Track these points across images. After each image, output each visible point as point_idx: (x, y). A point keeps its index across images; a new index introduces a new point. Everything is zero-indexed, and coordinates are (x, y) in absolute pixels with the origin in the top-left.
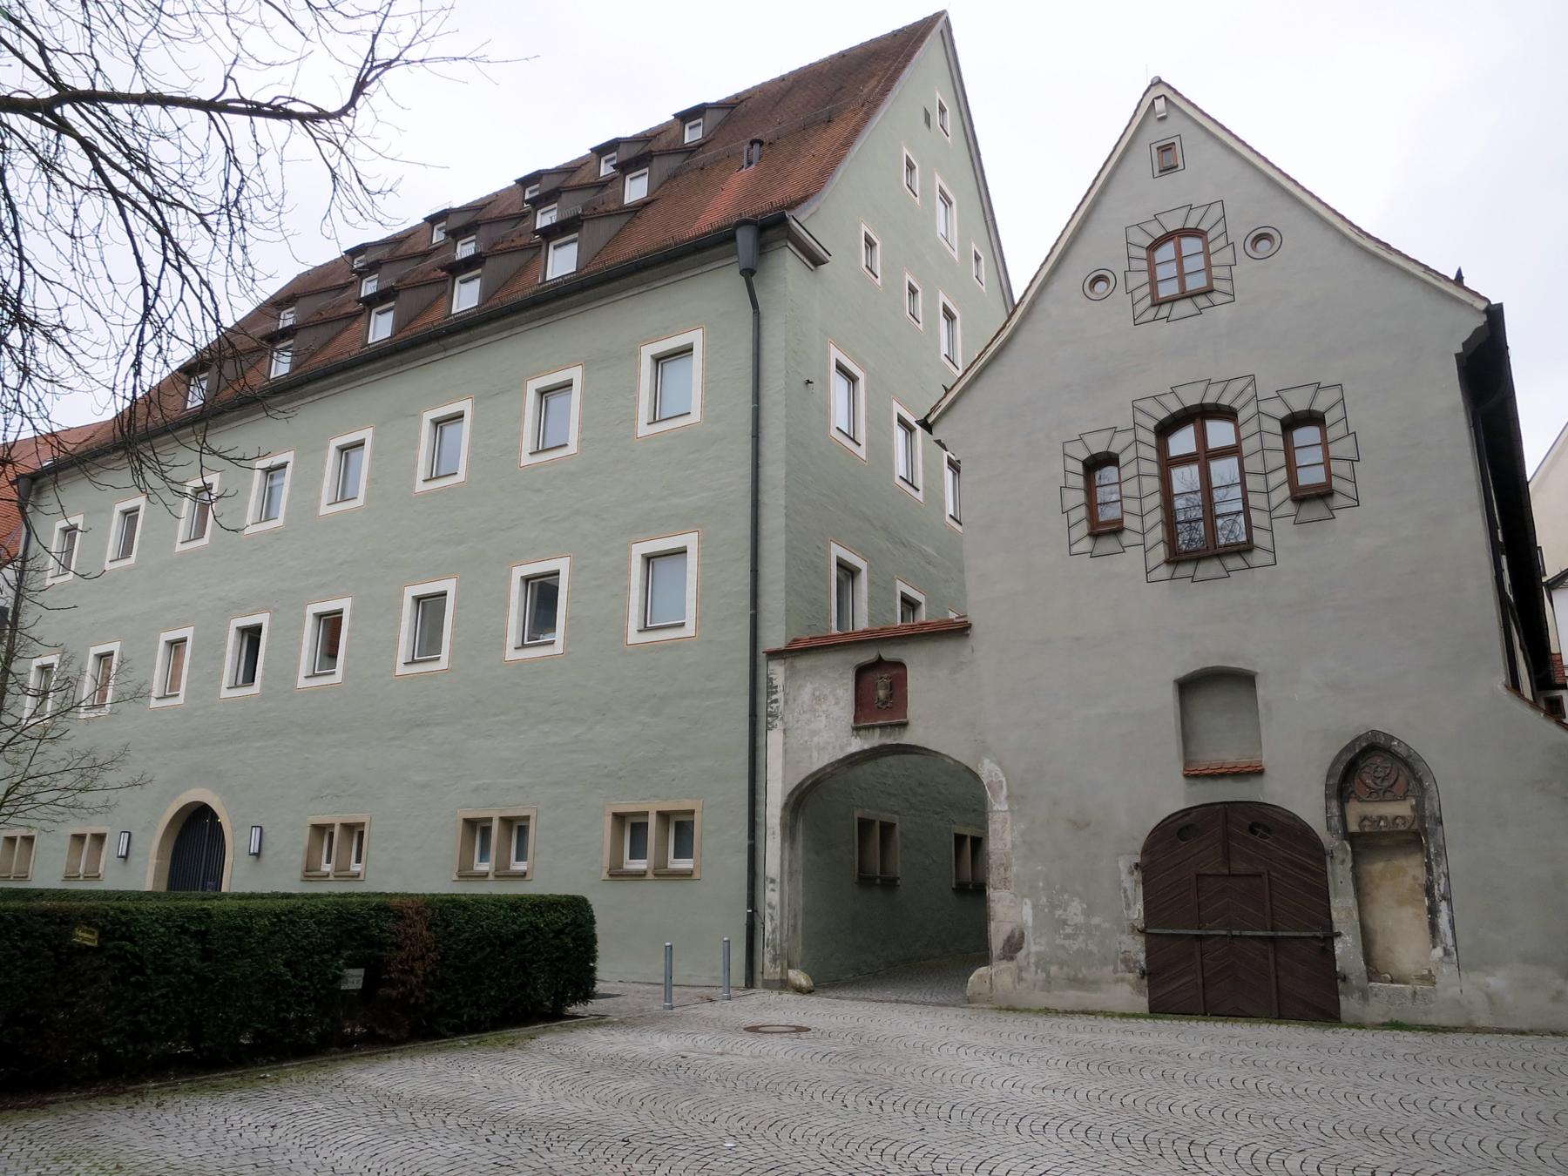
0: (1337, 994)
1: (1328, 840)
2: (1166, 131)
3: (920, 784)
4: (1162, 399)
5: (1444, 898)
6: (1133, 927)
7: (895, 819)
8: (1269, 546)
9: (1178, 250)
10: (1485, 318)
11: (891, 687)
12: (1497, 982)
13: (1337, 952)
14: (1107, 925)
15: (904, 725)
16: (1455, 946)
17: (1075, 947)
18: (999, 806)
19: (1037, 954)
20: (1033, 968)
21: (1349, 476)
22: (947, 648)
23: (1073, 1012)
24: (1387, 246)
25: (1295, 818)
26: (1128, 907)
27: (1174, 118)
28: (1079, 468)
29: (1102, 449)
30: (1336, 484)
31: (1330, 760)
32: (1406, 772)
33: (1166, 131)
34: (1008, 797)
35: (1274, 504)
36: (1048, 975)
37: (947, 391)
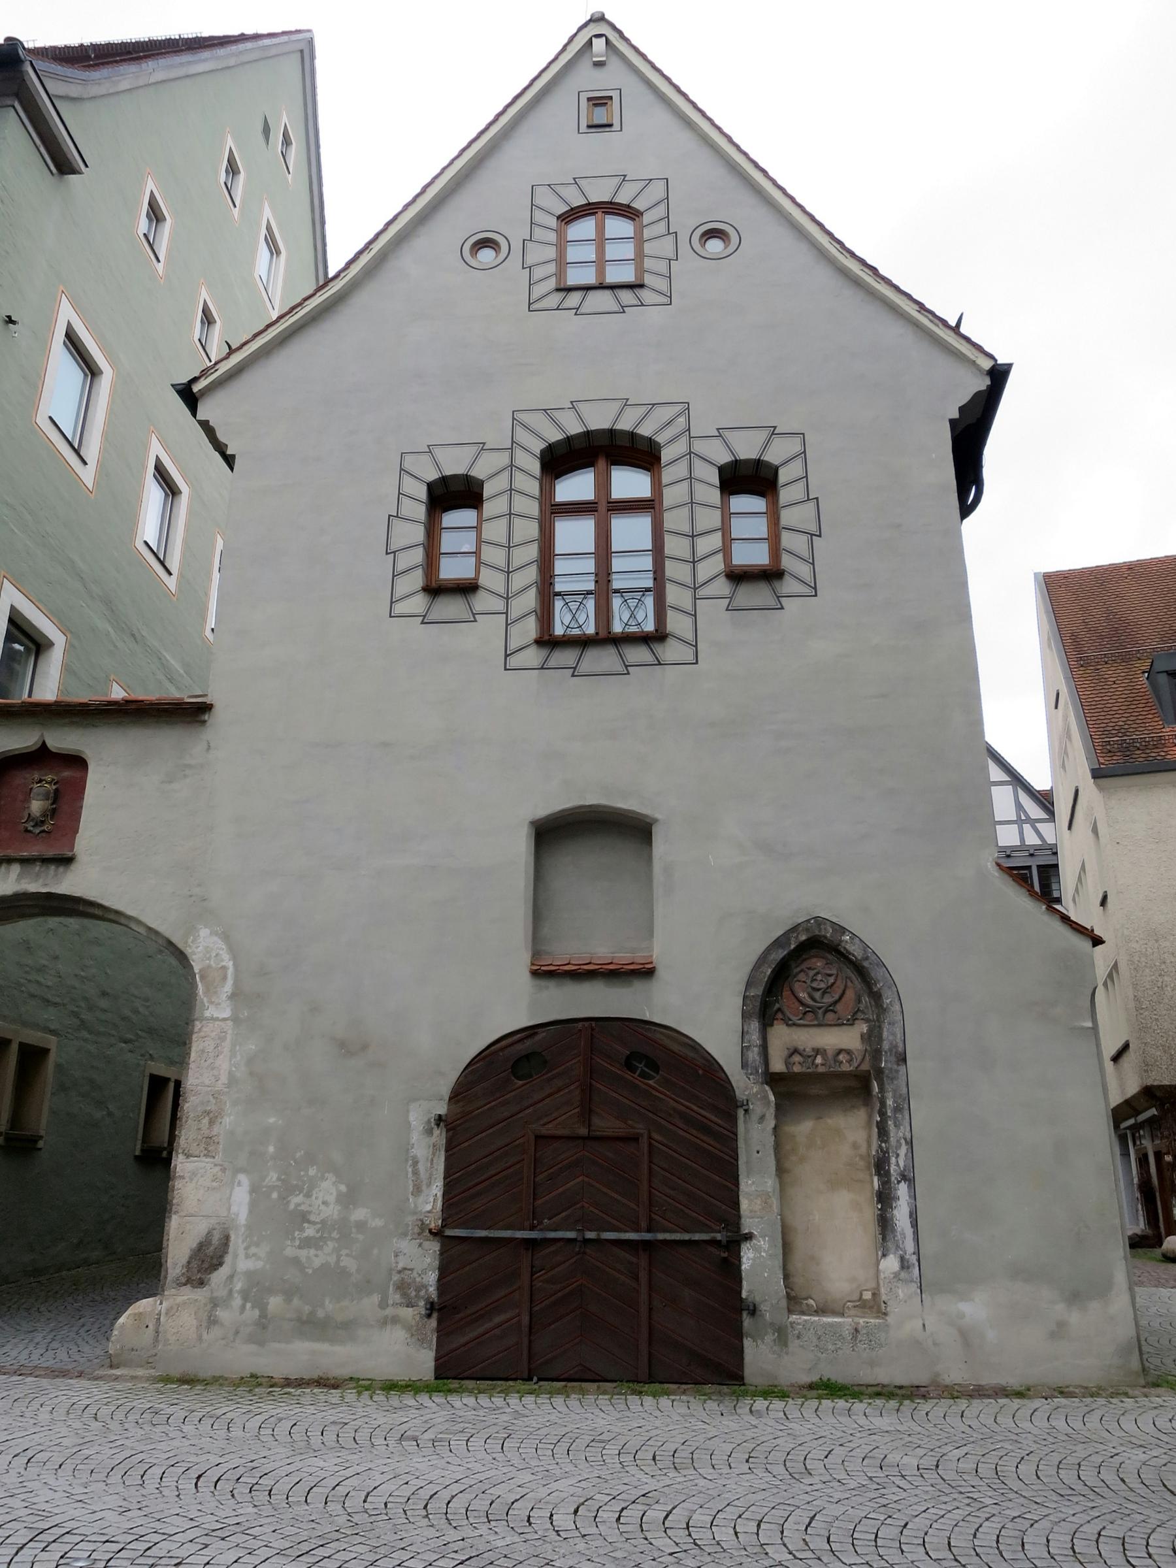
0: (739, 1335)
1: (744, 1084)
2: (598, 75)
3: (104, 994)
4: (557, 415)
5: (907, 1177)
6: (423, 1226)
7: (51, 1042)
8: (690, 636)
9: (601, 229)
10: (988, 382)
11: (56, 797)
12: (974, 1309)
13: (745, 1266)
14: (378, 1223)
15: (67, 861)
16: (917, 1253)
17: (317, 1263)
18: (215, 1011)
19: (249, 1274)
20: (237, 1301)
21: (806, 554)
22: (163, 741)
23: (300, 1383)
24: (874, 270)
25: (694, 1046)
26: (418, 1190)
27: (614, 64)
28: (422, 493)
29: (460, 470)
30: (787, 562)
31: (754, 958)
32: (858, 983)
33: (598, 75)
34: (233, 996)
35: (701, 578)
36: (263, 1315)
37: (232, 351)
